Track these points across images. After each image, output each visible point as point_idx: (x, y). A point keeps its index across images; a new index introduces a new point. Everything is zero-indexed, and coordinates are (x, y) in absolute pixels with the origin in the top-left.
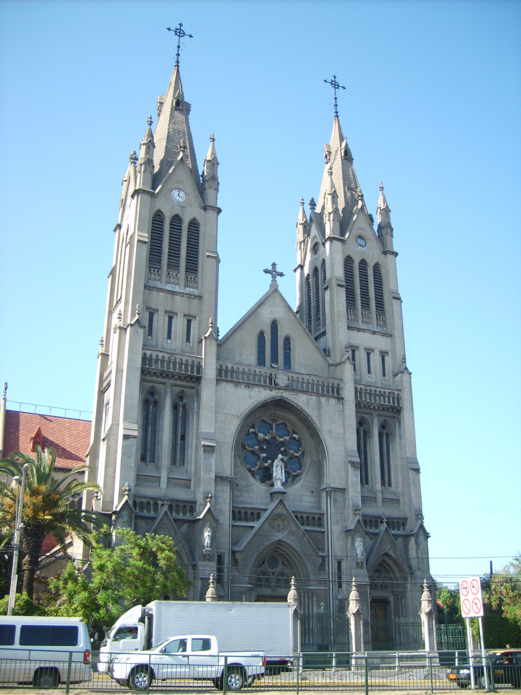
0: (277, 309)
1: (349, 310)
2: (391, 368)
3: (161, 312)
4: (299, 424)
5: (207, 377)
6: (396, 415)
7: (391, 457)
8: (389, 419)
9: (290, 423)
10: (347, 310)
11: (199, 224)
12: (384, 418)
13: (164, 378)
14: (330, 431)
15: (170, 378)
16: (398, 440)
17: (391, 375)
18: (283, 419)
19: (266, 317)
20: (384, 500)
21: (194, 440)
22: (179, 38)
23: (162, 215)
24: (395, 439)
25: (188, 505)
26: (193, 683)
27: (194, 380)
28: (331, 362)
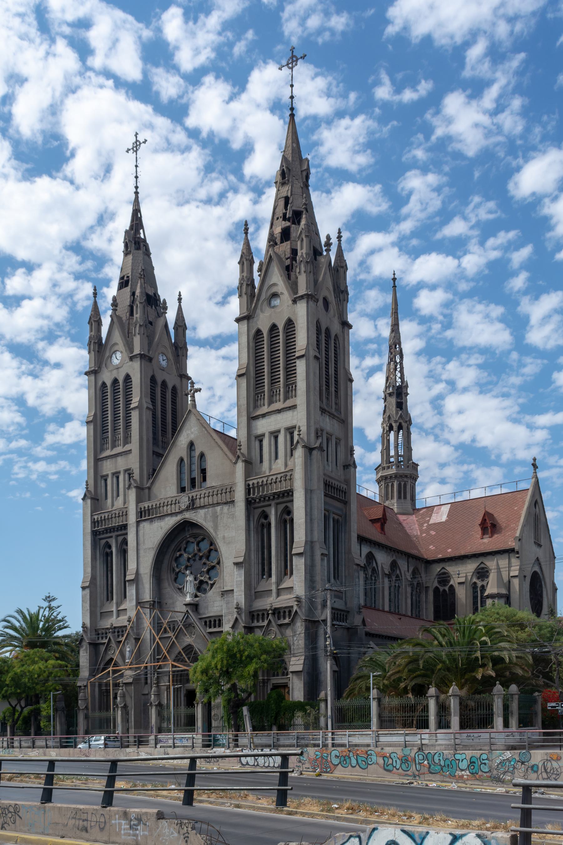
14: (224, 538)
15: (114, 531)
19: (183, 442)
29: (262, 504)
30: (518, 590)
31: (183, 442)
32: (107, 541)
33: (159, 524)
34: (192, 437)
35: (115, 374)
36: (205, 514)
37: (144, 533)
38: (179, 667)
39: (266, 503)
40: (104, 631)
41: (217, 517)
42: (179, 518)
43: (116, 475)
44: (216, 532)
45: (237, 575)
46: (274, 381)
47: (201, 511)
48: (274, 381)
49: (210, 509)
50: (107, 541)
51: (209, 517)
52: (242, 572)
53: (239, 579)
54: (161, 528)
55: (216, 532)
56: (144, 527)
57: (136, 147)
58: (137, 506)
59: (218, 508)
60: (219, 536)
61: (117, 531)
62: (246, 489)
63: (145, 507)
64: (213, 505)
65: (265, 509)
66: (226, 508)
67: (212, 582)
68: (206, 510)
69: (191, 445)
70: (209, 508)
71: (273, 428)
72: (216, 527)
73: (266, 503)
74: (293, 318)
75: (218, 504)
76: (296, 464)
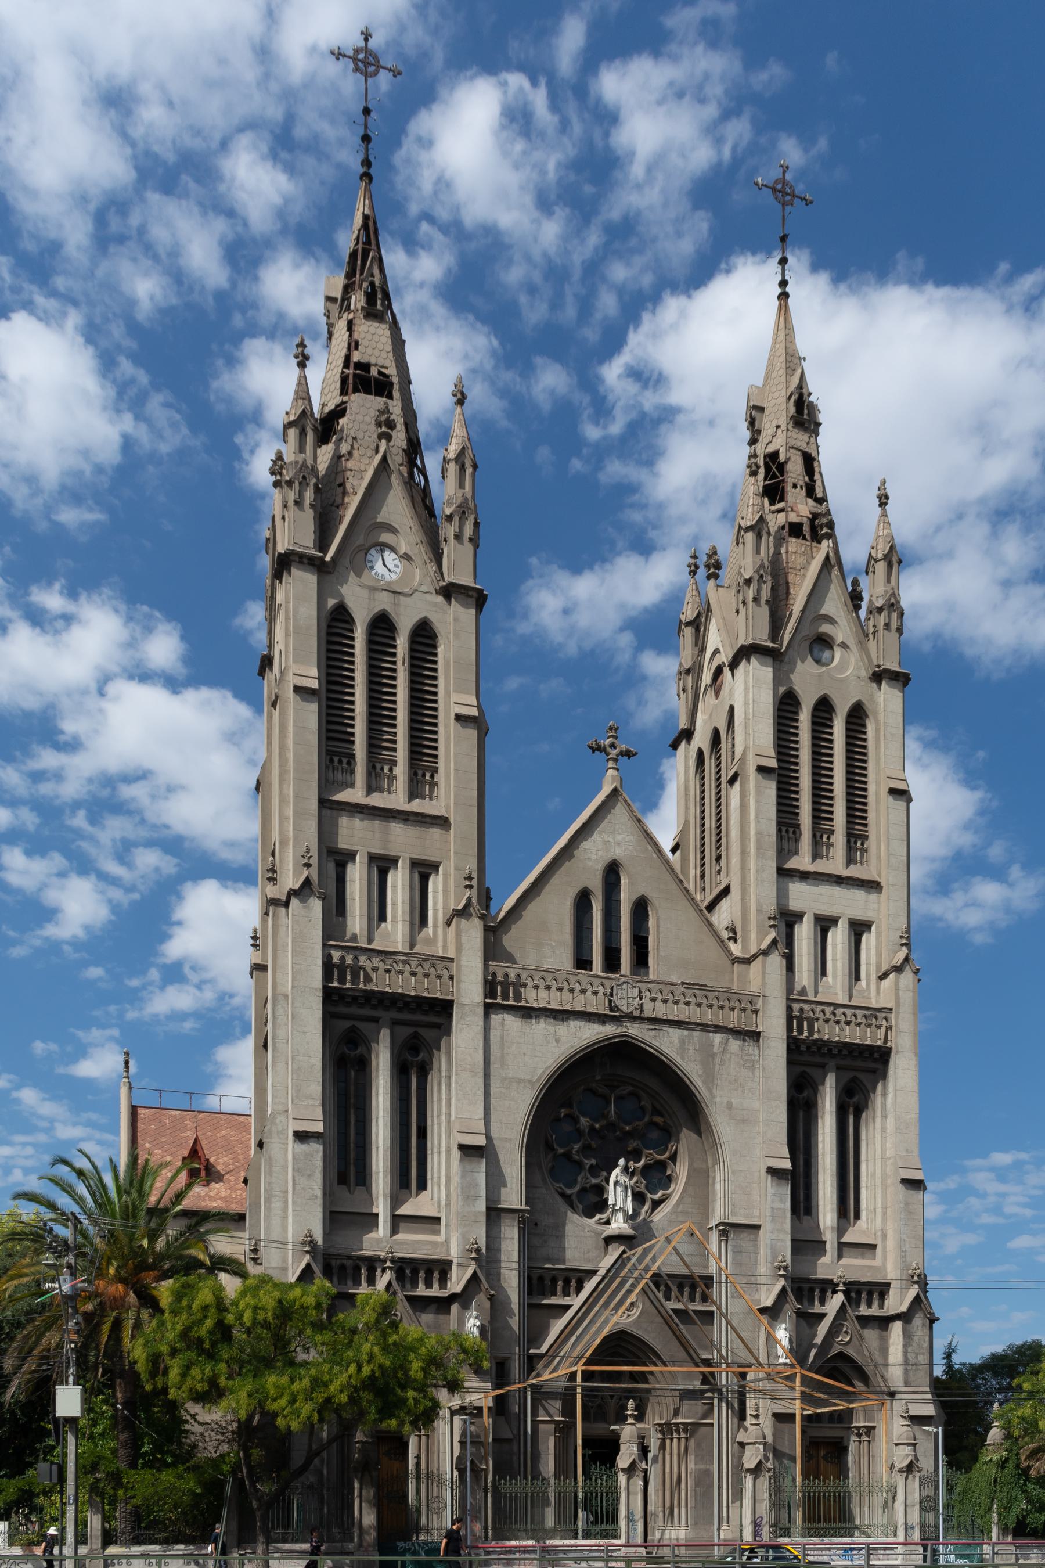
0: (619, 837)
1: (784, 829)
2: (873, 960)
5: (465, 1000)
6: (880, 1066)
13: (374, 1007)
14: (730, 1106)
15: (387, 1009)
16: (878, 1120)
17: (874, 977)
19: (594, 857)
23: (348, 618)
24: (874, 1118)
29: (806, 1058)
30: (545, 1302)
31: (594, 857)
32: (416, 1032)
33: (551, 1028)
34: (618, 853)
35: (383, 602)
36: (682, 1042)
37: (502, 1037)
38: (552, 1372)
39: (818, 1059)
40: (349, 1263)
41: (713, 1056)
42: (609, 1030)
43: (825, 924)
44: (710, 1090)
45: (774, 1195)
46: (821, 814)
47: (670, 1030)
48: (821, 814)
49: (695, 1033)
50: (416, 1032)
51: (691, 1051)
52: (787, 1191)
53: (778, 1205)
54: (557, 1041)
55: (710, 1090)
56: (503, 1024)
57: (785, 193)
58: (486, 967)
59: (717, 1038)
60: (718, 1099)
61: (400, 1010)
62: (486, 981)
63: (506, 975)
64: (705, 1027)
65: (361, 1026)
66: (735, 1044)
67: (656, 1197)
68: (686, 1033)
69: (612, 872)
70: (693, 1030)
71: (825, 910)
72: (710, 1077)
73: (818, 1059)
74: (868, 706)
75: (718, 1029)
76: (902, 1001)
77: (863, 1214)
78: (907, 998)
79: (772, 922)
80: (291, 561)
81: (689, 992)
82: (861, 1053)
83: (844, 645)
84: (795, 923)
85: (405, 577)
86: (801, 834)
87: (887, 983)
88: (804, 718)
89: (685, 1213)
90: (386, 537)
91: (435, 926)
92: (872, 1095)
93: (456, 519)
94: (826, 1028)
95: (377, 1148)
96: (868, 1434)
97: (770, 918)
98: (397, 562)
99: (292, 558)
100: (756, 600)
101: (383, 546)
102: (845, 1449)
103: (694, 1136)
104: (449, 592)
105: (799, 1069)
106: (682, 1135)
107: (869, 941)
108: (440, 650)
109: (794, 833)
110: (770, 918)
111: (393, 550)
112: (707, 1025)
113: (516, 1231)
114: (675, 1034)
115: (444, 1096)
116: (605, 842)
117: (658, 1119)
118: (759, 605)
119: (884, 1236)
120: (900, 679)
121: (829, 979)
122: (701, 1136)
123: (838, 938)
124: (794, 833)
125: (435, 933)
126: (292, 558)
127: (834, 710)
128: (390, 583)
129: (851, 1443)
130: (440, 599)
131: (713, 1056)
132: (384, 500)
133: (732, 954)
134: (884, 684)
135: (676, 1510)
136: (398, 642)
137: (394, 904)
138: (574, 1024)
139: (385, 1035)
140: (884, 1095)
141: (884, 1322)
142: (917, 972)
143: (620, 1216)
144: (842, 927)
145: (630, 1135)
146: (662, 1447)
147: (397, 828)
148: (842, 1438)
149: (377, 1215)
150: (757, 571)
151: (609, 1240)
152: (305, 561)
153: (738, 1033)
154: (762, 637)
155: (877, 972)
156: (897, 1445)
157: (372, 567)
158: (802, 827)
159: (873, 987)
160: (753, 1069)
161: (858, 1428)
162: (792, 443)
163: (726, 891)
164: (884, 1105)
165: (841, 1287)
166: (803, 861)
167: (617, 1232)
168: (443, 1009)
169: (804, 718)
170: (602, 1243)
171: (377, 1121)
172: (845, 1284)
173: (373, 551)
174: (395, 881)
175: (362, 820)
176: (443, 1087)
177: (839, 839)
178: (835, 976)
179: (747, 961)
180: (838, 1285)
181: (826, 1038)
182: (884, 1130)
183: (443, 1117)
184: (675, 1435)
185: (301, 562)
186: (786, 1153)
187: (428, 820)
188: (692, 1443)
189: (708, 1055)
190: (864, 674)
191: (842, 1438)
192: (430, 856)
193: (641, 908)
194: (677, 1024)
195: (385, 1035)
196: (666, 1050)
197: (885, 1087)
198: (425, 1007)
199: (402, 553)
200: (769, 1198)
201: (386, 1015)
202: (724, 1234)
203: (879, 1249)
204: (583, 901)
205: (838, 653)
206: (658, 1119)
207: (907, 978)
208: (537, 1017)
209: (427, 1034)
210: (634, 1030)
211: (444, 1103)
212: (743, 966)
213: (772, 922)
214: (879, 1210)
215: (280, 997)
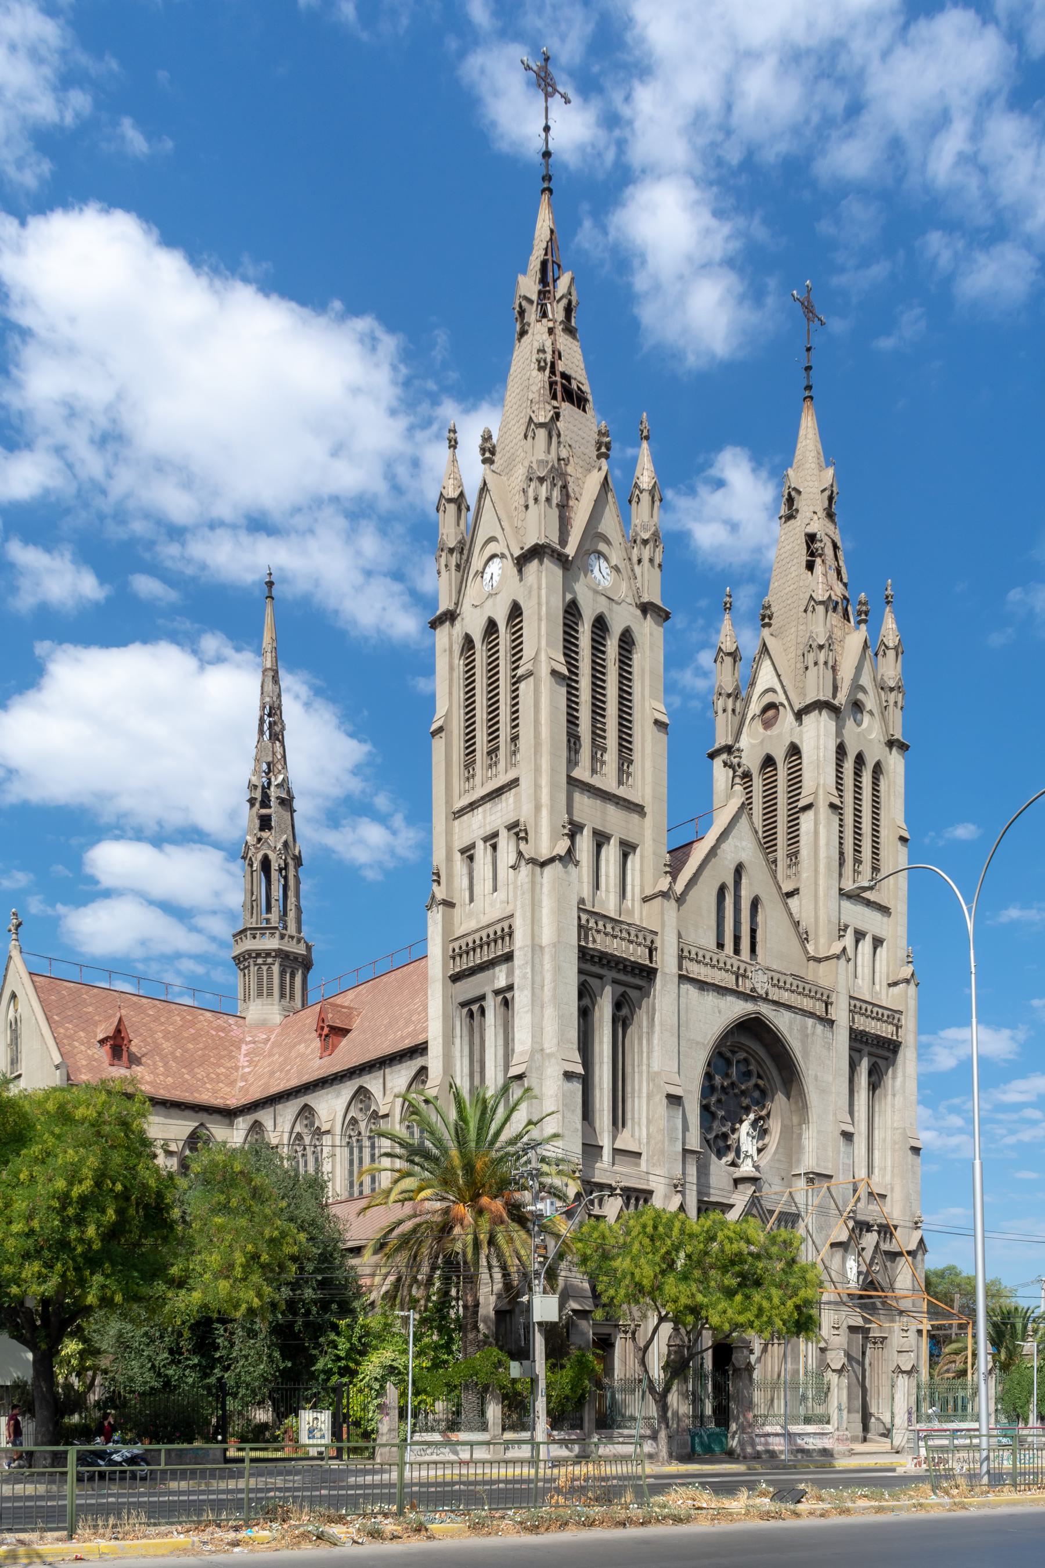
0: (744, 843)
1: (572, 740)
2: (884, 969)
3: (587, 832)
4: (769, 1063)
5: (667, 970)
6: (890, 1055)
7: (876, 1125)
8: (630, 991)
9: (756, 1060)
10: (569, 741)
11: (634, 644)
12: (622, 989)
13: (602, 966)
14: (816, 1078)
15: (610, 968)
16: (889, 1097)
17: (885, 984)
18: (747, 1052)
19: (729, 858)
20: (616, 1151)
21: (645, 1084)
22: (546, 101)
23: (576, 613)
24: (885, 1096)
25: (790, 1219)
26: (294, 1482)
27: (645, 974)
28: (812, 953)
35: (602, 606)
41: (807, 1036)
54: (720, 1012)
59: (810, 1022)
66: (820, 1028)
68: (793, 1015)
77: (629, 1123)
78: (912, 1004)
79: (668, 869)
80: (545, 553)
81: (795, 983)
82: (633, 969)
83: (871, 713)
84: (603, 843)
85: (615, 586)
86: (580, 746)
87: (895, 990)
88: (612, 647)
89: (779, 1160)
90: (602, 547)
91: (633, 900)
92: (598, 998)
93: (651, 544)
94: (599, 938)
95: (601, 1089)
96: (882, 1343)
97: (665, 865)
98: (608, 571)
99: (546, 550)
100: (548, 500)
101: (600, 554)
102: (612, 1346)
103: (785, 1099)
104: (646, 608)
105: (584, 977)
106: (776, 1097)
107: (634, 862)
108: (635, 657)
109: (575, 743)
110: (665, 865)
111: (606, 559)
112: (805, 1011)
113: (695, 1169)
114: (787, 1015)
115: (645, 1049)
116: (736, 846)
117: (760, 1082)
118: (550, 506)
119: (892, 1189)
120: (903, 747)
121: (860, 981)
122: (789, 1099)
123: (611, 853)
124: (575, 743)
125: (633, 905)
126: (546, 550)
127: (864, 764)
128: (605, 589)
129: (618, 1339)
130: (638, 612)
131: (807, 1036)
132: (603, 513)
133: (808, 953)
134: (894, 750)
135: (776, 1401)
136: (609, 643)
137: (607, 876)
138: (730, 999)
139: (608, 990)
140: (894, 1078)
141: (894, 1256)
142: (917, 985)
143: (749, 1161)
144: (868, 939)
145: (743, 1093)
146: (765, 1350)
147: (611, 809)
148: (610, 1335)
149: (602, 1147)
150: (827, 640)
151: (737, 1182)
152: (556, 555)
153: (820, 1019)
154: (825, 696)
155: (888, 979)
156: (899, 1352)
157: (592, 571)
158: (582, 739)
159: (884, 991)
160: (829, 1049)
161: (875, 1338)
162: (827, 531)
163: (514, 783)
164: (893, 1087)
165: (875, 1228)
166: (582, 772)
167: (745, 1175)
168: (648, 974)
169: (612, 647)
170: (732, 1182)
171: (601, 1067)
172: (878, 1226)
173: (592, 556)
174: (607, 856)
175: (589, 798)
176: (645, 1042)
177: (611, 757)
178: (863, 979)
179: (819, 960)
180: (615, 1189)
181: (861, 1028)
182: (893, 1106)
183: (644, 1067)
184: (776, 1341)
185: (552, 556)
186: (577, 1058)
187: (631, 806)
188: (789, 1346)
189: (805, 1036)
190: (883, 739)
191: (610, 1335)
192: (631, 839)
193: (755, 904)
194: (788, 1007)
195: (608, 990)
196: (782, 1028)
197: (894, 1072)
198: (637, 971)
199: (613, 563)
200: (842, 1155)
201: (610, 974)
202: (811, 1181)
203: (888, 1198)
204: (722, 890)
205: (866, 719)
206: (760, 1082)
207: (912, 988)
208: (708, 990)
209: (633, 994)
210: (765, 1009)
211: (645, 1055)
212: (816, 964)
213: (668, 869)
214: (889, 1168)
215: (537, 948)
